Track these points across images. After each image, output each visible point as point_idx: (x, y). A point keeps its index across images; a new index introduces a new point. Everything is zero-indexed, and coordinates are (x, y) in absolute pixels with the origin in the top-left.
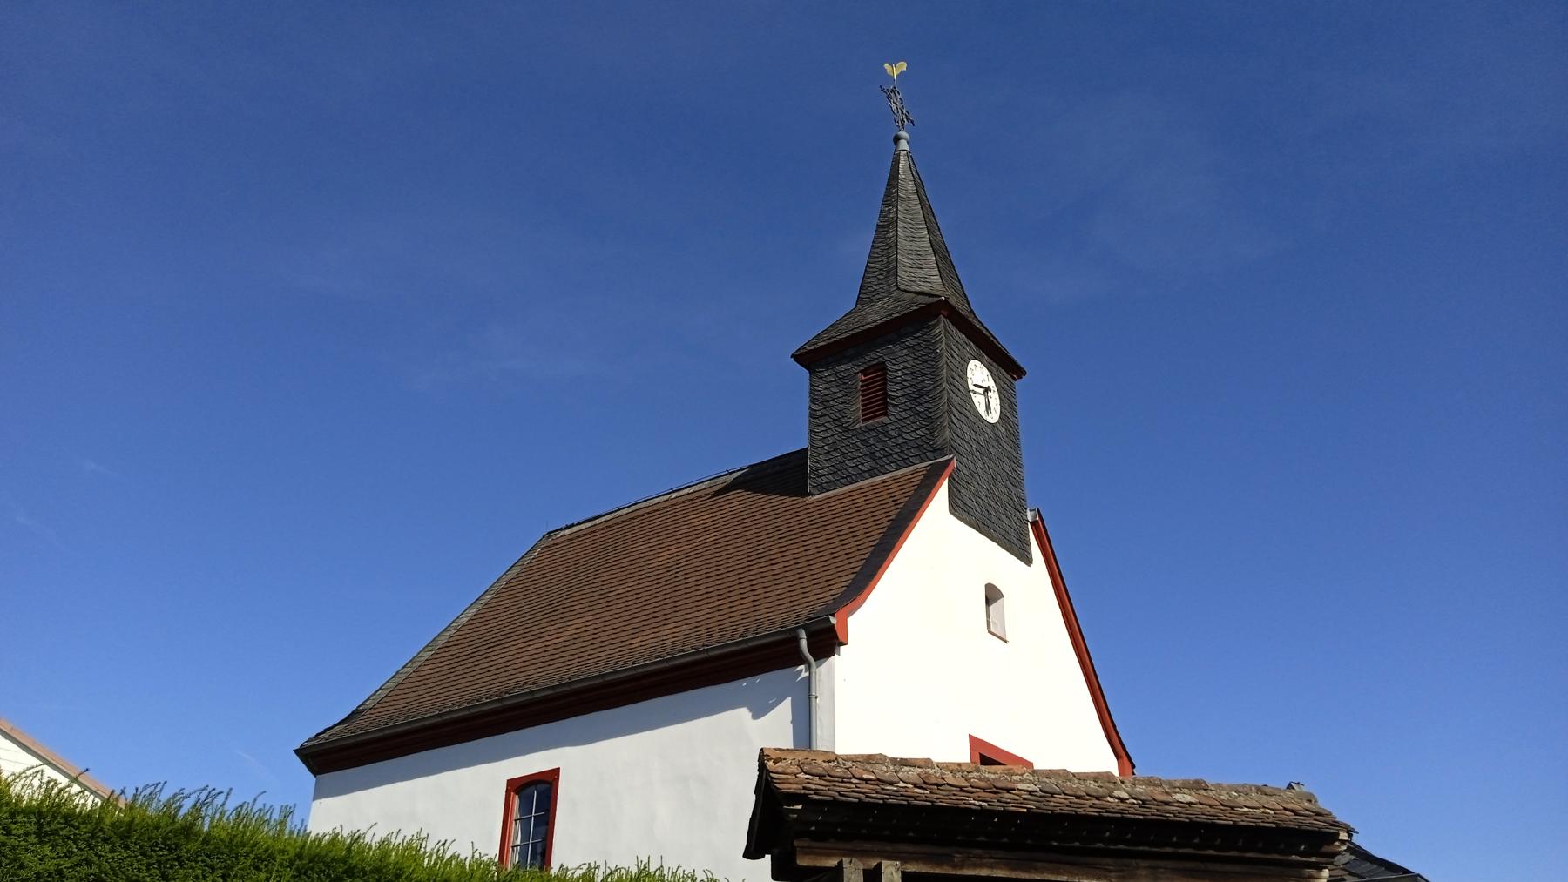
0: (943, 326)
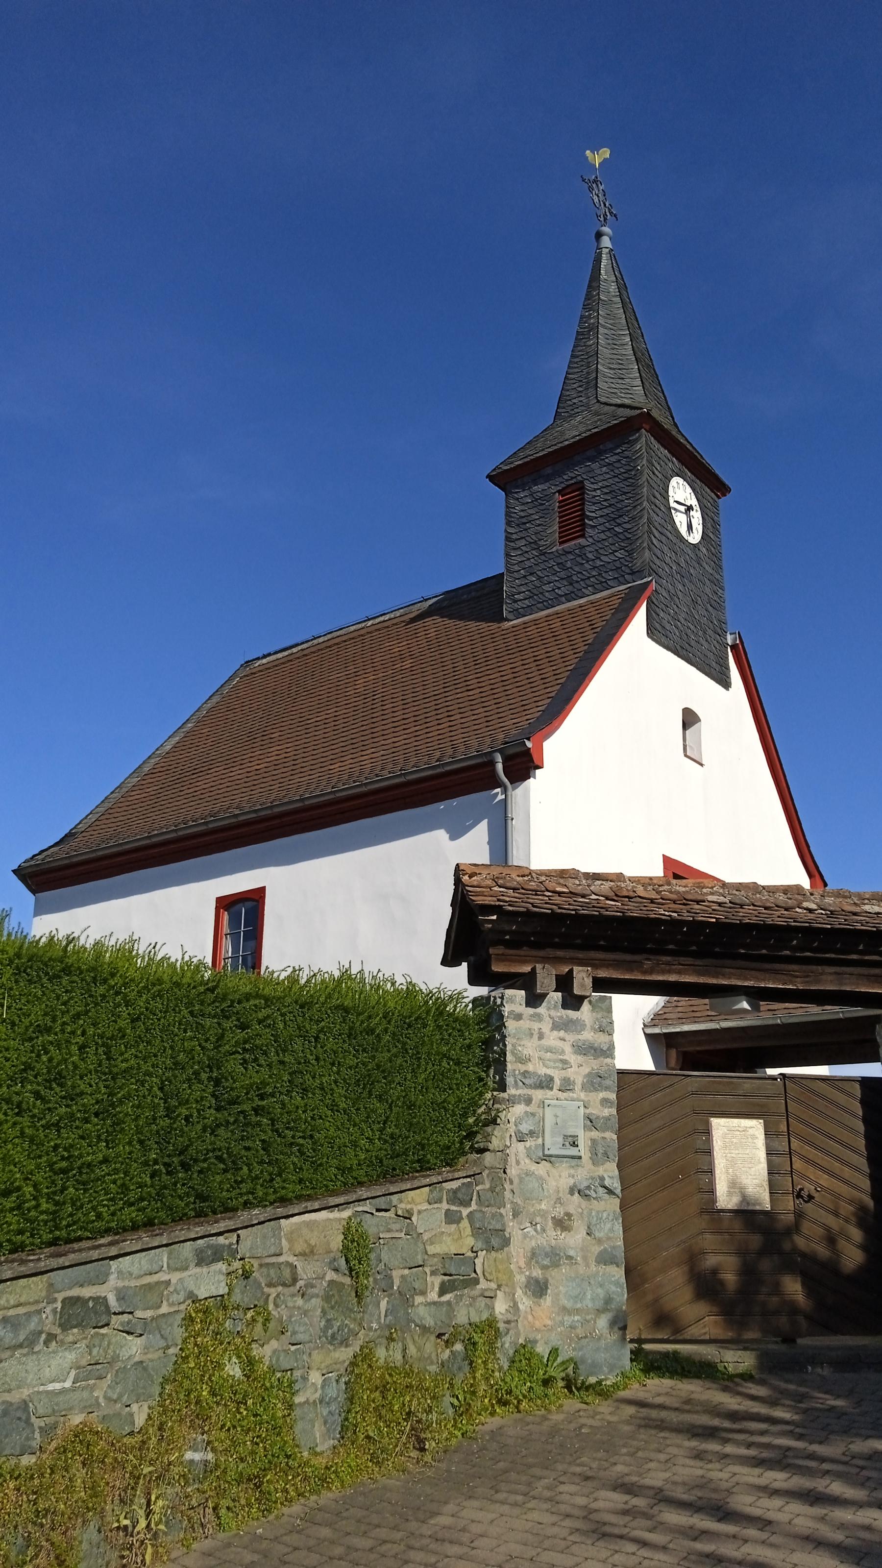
0: (644, 440)
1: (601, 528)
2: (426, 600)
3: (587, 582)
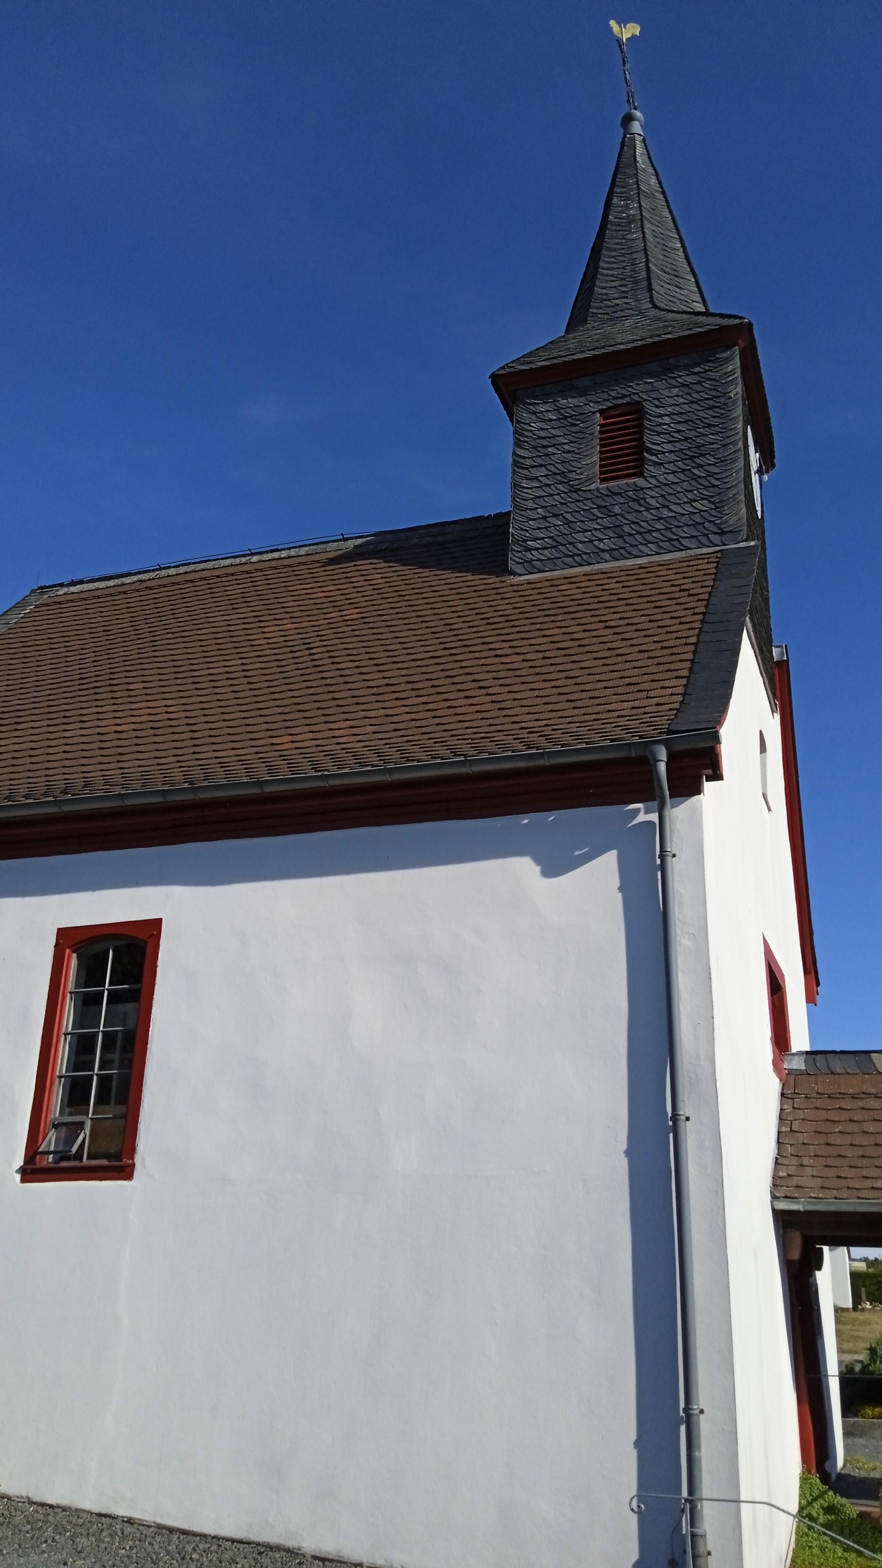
1: (671, 467)
2: (345, 540)
3: (648, 537)
